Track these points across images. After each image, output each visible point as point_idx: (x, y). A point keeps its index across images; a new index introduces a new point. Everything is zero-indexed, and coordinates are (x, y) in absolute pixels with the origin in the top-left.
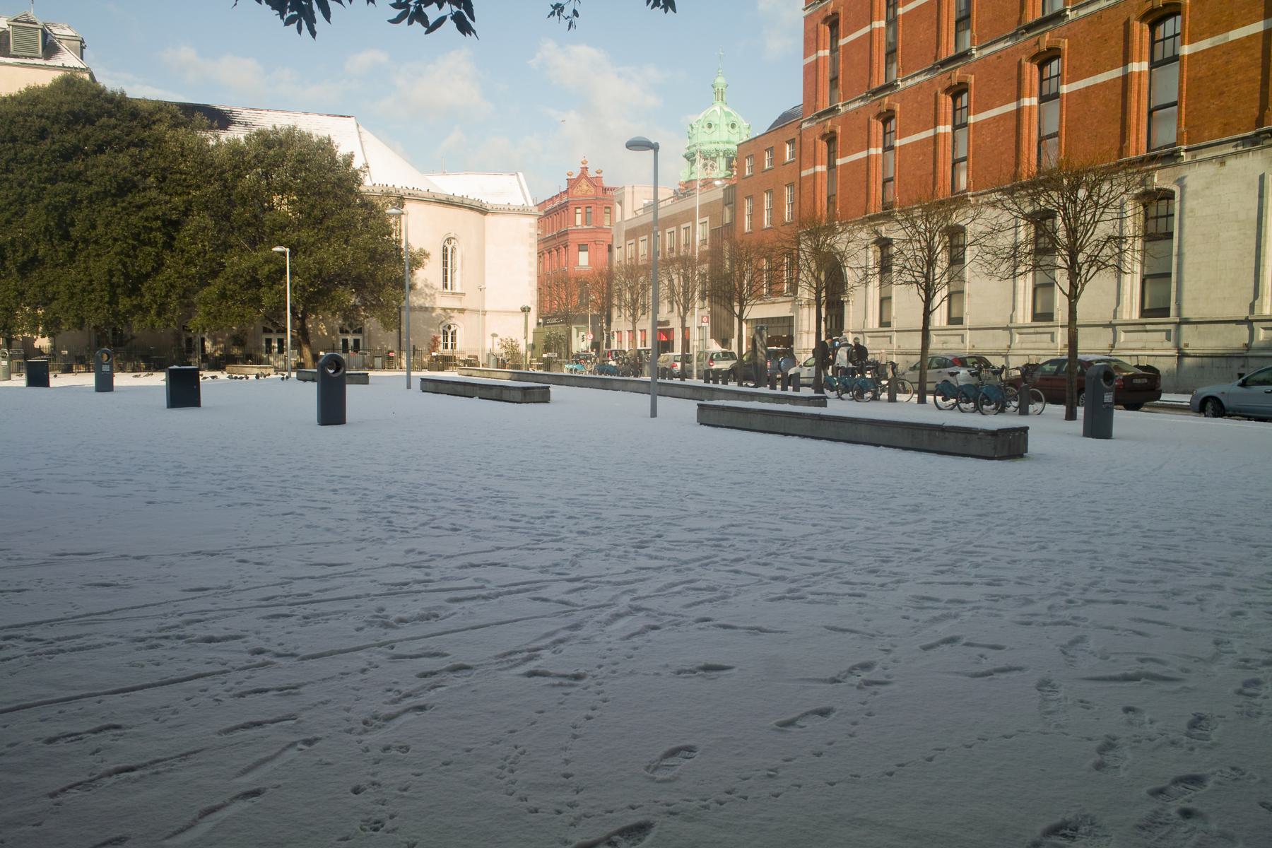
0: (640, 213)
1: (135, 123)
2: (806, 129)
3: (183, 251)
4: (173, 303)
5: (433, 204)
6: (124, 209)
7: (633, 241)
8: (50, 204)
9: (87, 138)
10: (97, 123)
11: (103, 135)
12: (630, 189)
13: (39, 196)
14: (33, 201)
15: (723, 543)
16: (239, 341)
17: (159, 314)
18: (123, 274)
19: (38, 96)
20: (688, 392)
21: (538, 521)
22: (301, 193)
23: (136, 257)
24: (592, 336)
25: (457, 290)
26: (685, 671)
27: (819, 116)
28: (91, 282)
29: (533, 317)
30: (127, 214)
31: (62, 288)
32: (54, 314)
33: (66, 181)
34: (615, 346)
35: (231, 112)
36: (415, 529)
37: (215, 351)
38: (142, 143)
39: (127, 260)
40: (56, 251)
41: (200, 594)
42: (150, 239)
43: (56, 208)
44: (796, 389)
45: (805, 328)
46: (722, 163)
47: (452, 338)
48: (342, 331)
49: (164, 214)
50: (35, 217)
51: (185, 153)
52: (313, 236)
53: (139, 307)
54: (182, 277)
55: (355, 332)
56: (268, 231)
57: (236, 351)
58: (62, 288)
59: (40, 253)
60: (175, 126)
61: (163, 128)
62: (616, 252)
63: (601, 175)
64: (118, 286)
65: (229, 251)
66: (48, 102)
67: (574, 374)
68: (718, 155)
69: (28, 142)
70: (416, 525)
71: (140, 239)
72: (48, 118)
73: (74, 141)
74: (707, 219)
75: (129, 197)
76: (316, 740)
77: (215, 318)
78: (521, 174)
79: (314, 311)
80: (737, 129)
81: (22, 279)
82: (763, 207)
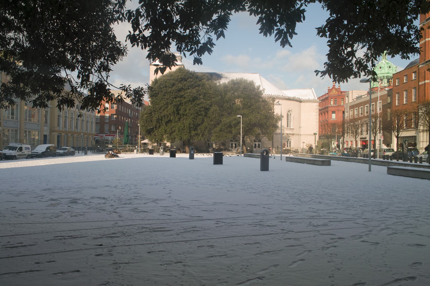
0: (355, 100)
1: (197, 80)
2: (421, 67)
3: (209, 117)
4: (206, 132)
5: (284, 100)
6: (194, 105)
7: (352, 110)
8: (175, 104)
9: (185, 85)
10: (188, 81)
11: (189, 84)
12: (351, 92)
13: (172, 102)
14: (170, 104)
15: (410, 212)
16: (223, 144)
17: (202, 136)
18: (193, 124)
19: (172, 74)
20: (379, 163)
21: (345, 202)
22: (244, 98)
23: (197, 119)
24: (337, 143)
25: (292, 128)
26: (410, 245)
27: (426, 62)
28: (184, 127)
29: (317, 136)
30: (195, 107)
31: (176, 129)
32: (174, 136)
33: (179, 98)
34: (345, 146)
35: (222, 74)
36: (308, 202)
37: (216, 147)
38: (199, 86)
39: (194, 120)
40: (175, 118)
41: (258, 215)
42: (201, 114)
43: (176, 106)
44: (421, 162)
45: (422, 140)
46: (385, 81)
47: (290, 143)
48: (255, 141)
49: (205, 106)
50: (171, 109)
51: (211, 88)
52: (248, 112)
53: (197, 134)
54: (209, 125)
55: (258, 141)
56: (234, 110)
57: (222, 147)
58: (176, 129)
59: (171, 119)
60: (208, 80)
61: (205, 81)
62: (346, 114)
63: (340, 87)
64: (192, 128)
65: (223, 117)
66: (175, 76)
67: (333, 156)
68: (384, 78)
69: (170, 87)
70: (308, 201)
71: (198, 114)
72: (175, 80)
73: (182, 86)
74: (381, 101)
75: (196, 102)
76: (311, 251)
77: (218, 137)
78: (313, 89)
79: (247, 135)
80: (391, 68)
81: (166, 126)
82: (403, 96)
